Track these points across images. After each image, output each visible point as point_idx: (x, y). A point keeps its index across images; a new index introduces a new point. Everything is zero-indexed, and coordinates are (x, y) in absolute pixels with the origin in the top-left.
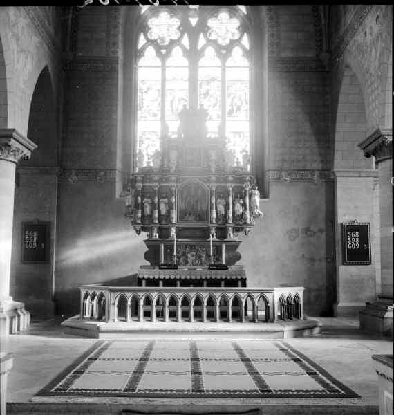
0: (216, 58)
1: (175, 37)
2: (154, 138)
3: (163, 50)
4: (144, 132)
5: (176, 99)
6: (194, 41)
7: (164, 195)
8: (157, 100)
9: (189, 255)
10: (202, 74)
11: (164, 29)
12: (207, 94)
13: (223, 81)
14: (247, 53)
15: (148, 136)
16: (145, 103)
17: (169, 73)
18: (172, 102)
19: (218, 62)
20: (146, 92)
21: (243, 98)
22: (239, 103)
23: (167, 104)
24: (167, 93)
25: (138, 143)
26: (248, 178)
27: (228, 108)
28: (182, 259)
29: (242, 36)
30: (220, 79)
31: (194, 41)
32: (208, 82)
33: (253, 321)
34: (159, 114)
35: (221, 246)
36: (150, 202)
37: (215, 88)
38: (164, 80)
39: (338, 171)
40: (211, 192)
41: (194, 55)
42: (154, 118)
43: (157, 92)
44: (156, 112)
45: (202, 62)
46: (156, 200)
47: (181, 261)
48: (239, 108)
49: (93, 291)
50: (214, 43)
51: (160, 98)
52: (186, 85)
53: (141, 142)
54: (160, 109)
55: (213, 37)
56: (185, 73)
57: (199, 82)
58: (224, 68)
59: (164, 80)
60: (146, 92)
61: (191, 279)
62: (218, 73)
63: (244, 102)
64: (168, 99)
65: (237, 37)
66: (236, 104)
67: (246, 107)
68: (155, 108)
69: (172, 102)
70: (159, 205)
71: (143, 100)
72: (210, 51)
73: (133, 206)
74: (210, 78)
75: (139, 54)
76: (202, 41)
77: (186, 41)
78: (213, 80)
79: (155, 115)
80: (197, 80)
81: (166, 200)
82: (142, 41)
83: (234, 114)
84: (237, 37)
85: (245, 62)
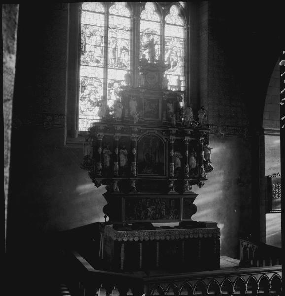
0: (155, 13)
2: (96, 84)
4: (87, 77)
5: (119, 47)
7: (124, 146)
8: (99, 46)
9: (149, 209)
10: (143, 26)
15: (90, 81)
16: (88, 48)
17: (112, 21)
18: (115, 49)
19: (157, 18)
20: (88, 37)
21: (179, 55)
22: (175, 59)
23: (110, 51)
24: (110, 40)
25: (81, 88)
26: (119, 128)
28: (143, 213)
30: (159, 34)
34: (102, 61)
35: (179, 200)
36: (111, 153)
38: (107, 28)
39: (268, 130)
40: (170, 144)
42: (95, 64)
43: (99, 39)
44: (98, 59)
46: (117, 151)
47: (142, 215)
49: (260, 276)
51: (102, 45)
52: (128, 36)
53: (84, 88)
54: (103, 55)
56: (127, 23)
57: (140, 34)
58: (163, 23)
59: (107, 28)
60: (88, 37)
61: (170, 239)
63: (179, 59)
66: (172, 60)
67: (181, 63)
68: (98, 53)
69: (115, 49)
70: (119, 156)
71: (86, 44)
73: (91, 156)
74: (150, 30)
79: (97, 61)
80: (139, 32)
81: (126, 151)
83: (171, 68)
85: (180, 21)
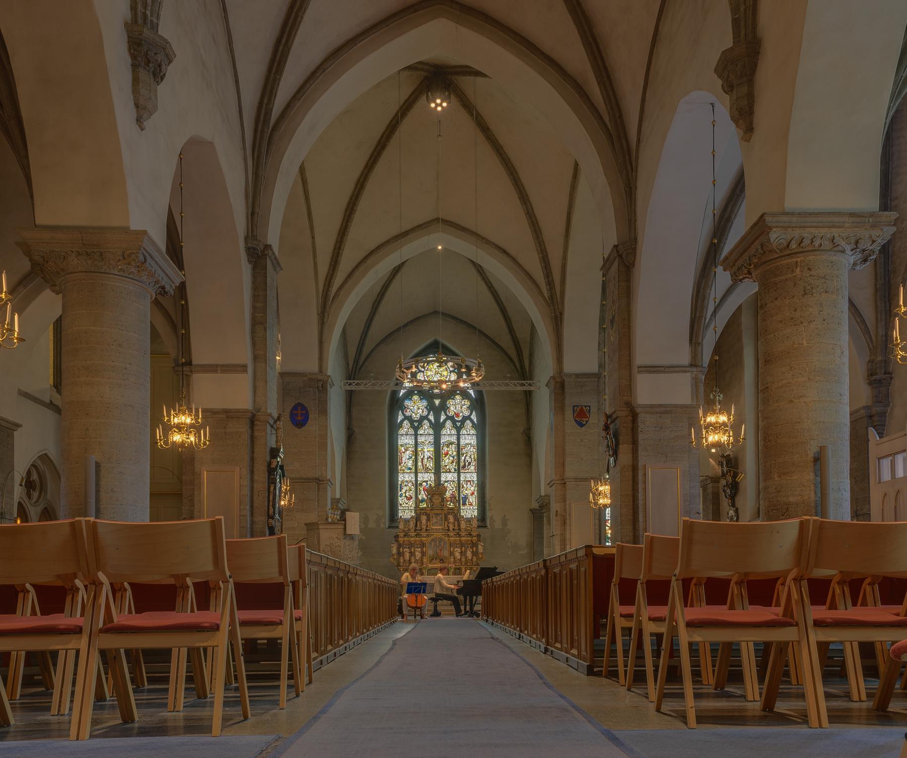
1: (467, 413)
3: (416, 425)
6: (437, 417)
11: (458, 407)
12: (446, 454)
13: (458, 444)
14: (474, 425)
27: (462, 464)
29: (471, 414)
31: (437, 417)
32: (448, 446)
33: (70, 723)
37: (452, 450)
41: (437, 427)
45: (444, 432)
48: (469, 464)
50: (409, 419)
53: (401, 489)
55: (408, 414)
56: (431, 439)
62: (454, 439)
64: (420, 457)
65: (425, 413)
72: (449, 424)
75: (400, 425)
76: (443, 417)
77: (431, 417)
78: (452, 443)
79: (410, 469)
82: (400, 418)
84: (425, 413)
